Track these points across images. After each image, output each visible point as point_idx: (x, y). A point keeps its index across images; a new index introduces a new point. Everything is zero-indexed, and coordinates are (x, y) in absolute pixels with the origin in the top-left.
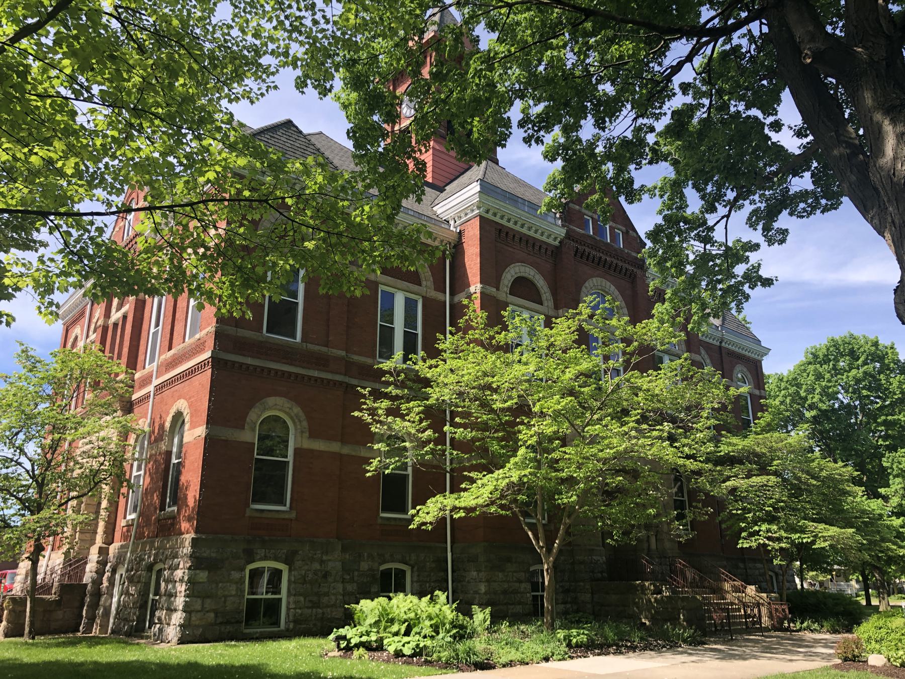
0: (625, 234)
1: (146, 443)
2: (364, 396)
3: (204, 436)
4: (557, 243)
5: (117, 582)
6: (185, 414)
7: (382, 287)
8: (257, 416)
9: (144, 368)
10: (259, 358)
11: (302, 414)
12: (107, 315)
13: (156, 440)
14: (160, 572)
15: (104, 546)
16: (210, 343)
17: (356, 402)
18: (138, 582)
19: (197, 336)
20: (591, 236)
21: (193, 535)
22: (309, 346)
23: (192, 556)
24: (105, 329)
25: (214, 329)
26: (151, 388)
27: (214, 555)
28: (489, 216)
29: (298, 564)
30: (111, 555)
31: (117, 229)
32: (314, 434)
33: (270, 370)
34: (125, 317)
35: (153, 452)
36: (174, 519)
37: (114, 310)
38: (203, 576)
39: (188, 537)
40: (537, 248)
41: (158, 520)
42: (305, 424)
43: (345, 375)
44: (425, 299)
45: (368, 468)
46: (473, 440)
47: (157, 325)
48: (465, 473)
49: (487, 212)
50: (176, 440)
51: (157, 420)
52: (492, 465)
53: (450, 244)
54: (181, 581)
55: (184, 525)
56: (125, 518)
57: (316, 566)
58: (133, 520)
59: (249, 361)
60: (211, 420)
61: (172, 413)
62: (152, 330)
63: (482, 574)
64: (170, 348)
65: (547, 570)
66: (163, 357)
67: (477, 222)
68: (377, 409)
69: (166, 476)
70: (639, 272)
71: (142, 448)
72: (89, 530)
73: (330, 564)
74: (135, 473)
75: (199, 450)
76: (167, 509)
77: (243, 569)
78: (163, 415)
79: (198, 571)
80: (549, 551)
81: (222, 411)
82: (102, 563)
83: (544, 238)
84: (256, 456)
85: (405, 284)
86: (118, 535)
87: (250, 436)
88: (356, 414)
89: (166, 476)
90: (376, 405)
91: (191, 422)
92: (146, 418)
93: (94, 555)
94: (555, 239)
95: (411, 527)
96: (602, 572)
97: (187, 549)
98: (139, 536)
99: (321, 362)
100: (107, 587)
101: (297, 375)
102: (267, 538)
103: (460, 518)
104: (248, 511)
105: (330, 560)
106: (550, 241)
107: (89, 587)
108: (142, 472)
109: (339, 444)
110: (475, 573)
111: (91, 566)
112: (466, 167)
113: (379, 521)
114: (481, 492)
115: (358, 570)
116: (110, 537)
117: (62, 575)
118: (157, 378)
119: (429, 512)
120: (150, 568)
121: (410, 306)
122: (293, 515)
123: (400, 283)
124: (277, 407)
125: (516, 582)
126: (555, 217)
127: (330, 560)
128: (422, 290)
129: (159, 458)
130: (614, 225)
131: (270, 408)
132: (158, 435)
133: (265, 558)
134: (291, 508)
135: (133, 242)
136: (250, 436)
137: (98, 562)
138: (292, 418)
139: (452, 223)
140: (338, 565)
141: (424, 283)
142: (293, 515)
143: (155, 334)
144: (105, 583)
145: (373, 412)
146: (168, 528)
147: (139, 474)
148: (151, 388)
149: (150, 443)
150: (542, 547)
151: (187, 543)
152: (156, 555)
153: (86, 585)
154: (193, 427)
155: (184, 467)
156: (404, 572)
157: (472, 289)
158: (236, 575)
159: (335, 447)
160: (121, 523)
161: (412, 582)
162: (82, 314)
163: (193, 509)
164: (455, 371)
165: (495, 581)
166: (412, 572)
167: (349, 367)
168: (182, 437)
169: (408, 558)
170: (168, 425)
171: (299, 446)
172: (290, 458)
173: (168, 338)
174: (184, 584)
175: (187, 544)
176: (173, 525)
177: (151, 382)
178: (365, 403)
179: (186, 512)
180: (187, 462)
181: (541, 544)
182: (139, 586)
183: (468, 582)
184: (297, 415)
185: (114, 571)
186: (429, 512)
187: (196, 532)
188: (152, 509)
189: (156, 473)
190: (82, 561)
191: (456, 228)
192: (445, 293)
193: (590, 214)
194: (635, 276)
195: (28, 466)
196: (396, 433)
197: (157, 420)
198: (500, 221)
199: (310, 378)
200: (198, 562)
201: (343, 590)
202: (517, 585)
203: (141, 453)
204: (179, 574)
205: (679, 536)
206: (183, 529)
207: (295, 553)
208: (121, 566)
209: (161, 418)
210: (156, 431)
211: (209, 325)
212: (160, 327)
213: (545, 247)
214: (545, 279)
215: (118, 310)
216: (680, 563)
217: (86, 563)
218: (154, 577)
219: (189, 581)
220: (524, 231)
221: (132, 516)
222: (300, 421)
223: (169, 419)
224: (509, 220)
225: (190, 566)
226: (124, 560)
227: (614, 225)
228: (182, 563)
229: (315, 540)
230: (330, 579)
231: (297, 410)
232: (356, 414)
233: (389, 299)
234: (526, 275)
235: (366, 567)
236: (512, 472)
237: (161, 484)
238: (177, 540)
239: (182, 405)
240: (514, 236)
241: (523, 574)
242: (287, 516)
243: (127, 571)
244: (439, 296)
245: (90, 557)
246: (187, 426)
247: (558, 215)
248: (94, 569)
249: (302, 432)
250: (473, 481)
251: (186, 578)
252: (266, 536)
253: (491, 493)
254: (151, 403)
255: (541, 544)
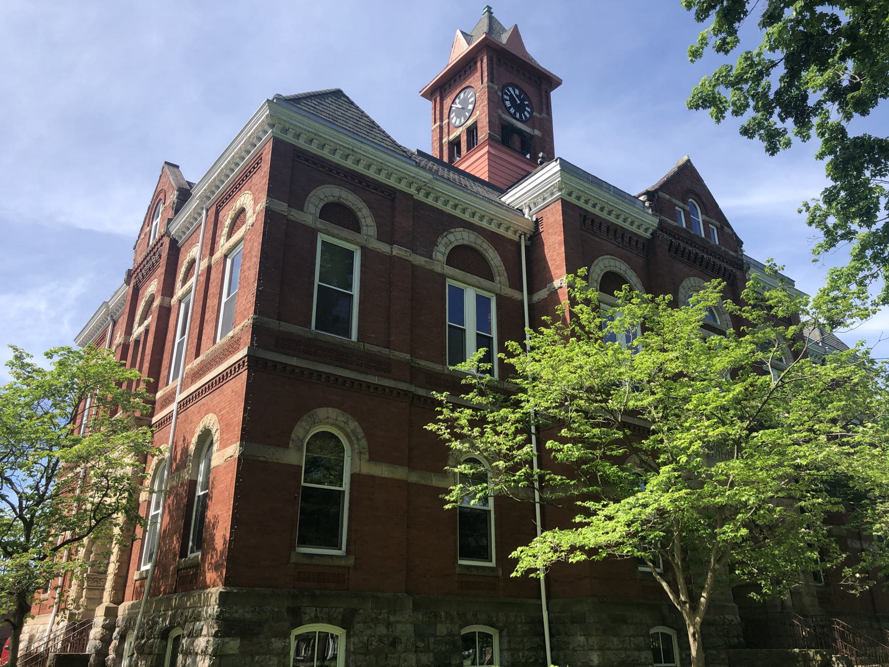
0: (720, 230)
1: (166, 473)
2: (440, 403)
3: (237, 455)
4: (648, 235)
5: (126, 654)
6: (213, 431)
7: (449, 282)
8: (305, 431)
9: (167, 384)
10: (307, 359)
11: (359, 430)
12: (129, 331)
13: (178, 469)
14: (177, 639)
15: (113, 605)
16: (247, 339)
17: (430, 410)
18: (150, 654)
19: (231, 334)
20: (683, 229)
21: (220, 588)
22: (368, 346)
23: (219, 618)
24: (125, 347)
25: (251, 321)
26: (174, 407)
27: (248, 616)
28: (572, 200)
29: (358, 627)
30: (120, 617)
31: (142, 236)
32: (375, 457)
33: (320, 374)
34: (147, 331)
35: (174, 483)
36: (197, 567)
37: (136, 325)
38: (233, 645)
39: (215, 592)
40: (627, 239)
41: (178, 570)
42: (364, 442)
43: (411, 383)
44: (499, 297)
45: (447, 498)
46: (581, 461)
47: (183, 334)
48: (579, 503)
49: (570, 194)
50: (202, 467)
51: (180, 443)
52: (614, 491)
53: (525, 235)
54: (204, 653)
55: (210, 576)
56: (138, 569)
57: (382, 630)
58: (147, 571)
59: (294, 361)
60: (247, 435)
61: (198, 432)
62: (178, 340)
63: (594, 641)
64: (197, 355)
65: (694, 635)
66: (189, 367)
67: (558, 206)
68: (458, 419)
69: (189, 512)
70: (738, 273)
71: (161, 482)
72: (95, 580)
73: (399, 626)
74: (152, 513)
75: (231, 475)
76: (191, 556)
77: (287, 635)
78: (188, 437)
79: (227, 639)
80: (694, 609)
81: (261, 424)
82: (109, 628)
83: (634, 229)
84: (303, 484)
85: (475, 279)
86: (129, 591)
87: (297, 457)
88: (431, 427)
89: (189, 512)
90: (456, 414)
91: (222, 440)
92: (167, 443)
93: (99, 618)
94: (646, 230)
95: (513, 575)
96: (738, 636)
97: (213, 609)
98: (154, 592)
99: (382, 366)
100: (113, 660)
101: (353, 381)
102: (318, 592)
103: (578, 562)
104: (293, 555)
105: (399, 622)
106: (641, 232)
107: (91, 659)
108: (160, 511)
109: (406, 469)
110: (582, 639)
111: (95, 632)
112: (525, 173)
113: (458, 570)
114: (607, 527)
115: (434, 635)
116: (120, 593)
117: (65, 642)
118: (180, 393)
119: (536, 555)
120: (165, 634)
121: (482, 304)
122: (351, 561)
123: (470, 277)
124: (328, 420)
125: (635, 649)
126: (644, 206)
127: (399, 622)
128: (496, 286)
129: (180, 490)
130: (708, 219)
131: (320, 422)
132: (180, 462)
133: (316, 620)
134: (348, 551)
135: (159, 245)
136: (297, 457)
137: (104, 627)
138: (347, 435)
139: (526, 211)
140: (410, 628)
141: (497, 278)
142: (351, 561)
143: (181, 344)
144: (112, 655)
145: (451, 423)
146: (189, 580)
147: (155, 510)
148: (174, 407)
149: (170, 473)
150: (685, 603)
151: (214, 599)
152: (173, 617)
153: (88, 656)
154: (223, 446)
155: (211, 498)
156: (490, 636)
157: (556, 283)
158: (277, 644)
159: (400, 473)
160: (134, 575)
161: (501, 650)
162: (102, 338)
163: (222, 553)
164: (553, 367)
165: (609, 649)
166: (501, 637)
167: (414, 374)
168: (210, 460)
169: (494, 619)
170: (192, 447)
171: (357, 471)
172: (346, 486)
173: (195, 344)
174: (207, 658)
175: (213, 600)
176: (196, 575)
177: (174, 399)
178: (441, 413)
179: (213, 558)
180: (215, 491)
181: (683, 598)
182: (150, 659)
183: (574, 650)
184: (353, 432)
185: (123, 638)
186: (536, 555)
187: (225, 584)
188: (171, 556)
189: (177, 509)
190: (87, 625)
191: (531, 216)
192: (522, 291)
193: (681, 205)
194: (735, 276)
195: (14, 499)
196: (481, 453)
197: (180, 443)
198: (585, 206)
199: (369, 385)
200: (227, 626)
201: (417, 663)
202: (637, 653)
203: (160, 486)
204: (201, 643)
205: (852, 587)
206: (208, 582)
207: (353, 612)
208: (130, 631)
209: (184, 440)
210: (179, 457)
211: (245, 318)
212: (186, 336)
213: (635, 239)
214: (639, 276)
215: (140, 325)
216: (838, 624)
217: (90, 627)
218: (170, 647)
219: (215, 654)
220: (612, 218)
221: (146, 567)
222: (358, 440)
223: (194, 440)
224: (594, 206)
225: (216, 632)
226: (135, 624)
227: (708, 219)
228: (205, 628)
229: (379, 594)
230: (400, 648)
231: (353, 425)
232: (431, 427)
233: (458, 296)
234: (617, 270)
235: (445, 631)
236: (656, 495)
237: (181, 523)
238: (200, 596)
239: (211, 420)
240: (601, 224)
241: (642, 639)
242: (343, 563)
243: (137, 638)
244: (515, 294)
245: (95, 620)
246: (215, 447)
247: (647, 204)
248: (99, 636)
249: (360, 453)
250: (589, 513)
251: (210, 650)
252: (319, 590)
253: (629, 525)
254: (173, 424)
255: (683, 598)
